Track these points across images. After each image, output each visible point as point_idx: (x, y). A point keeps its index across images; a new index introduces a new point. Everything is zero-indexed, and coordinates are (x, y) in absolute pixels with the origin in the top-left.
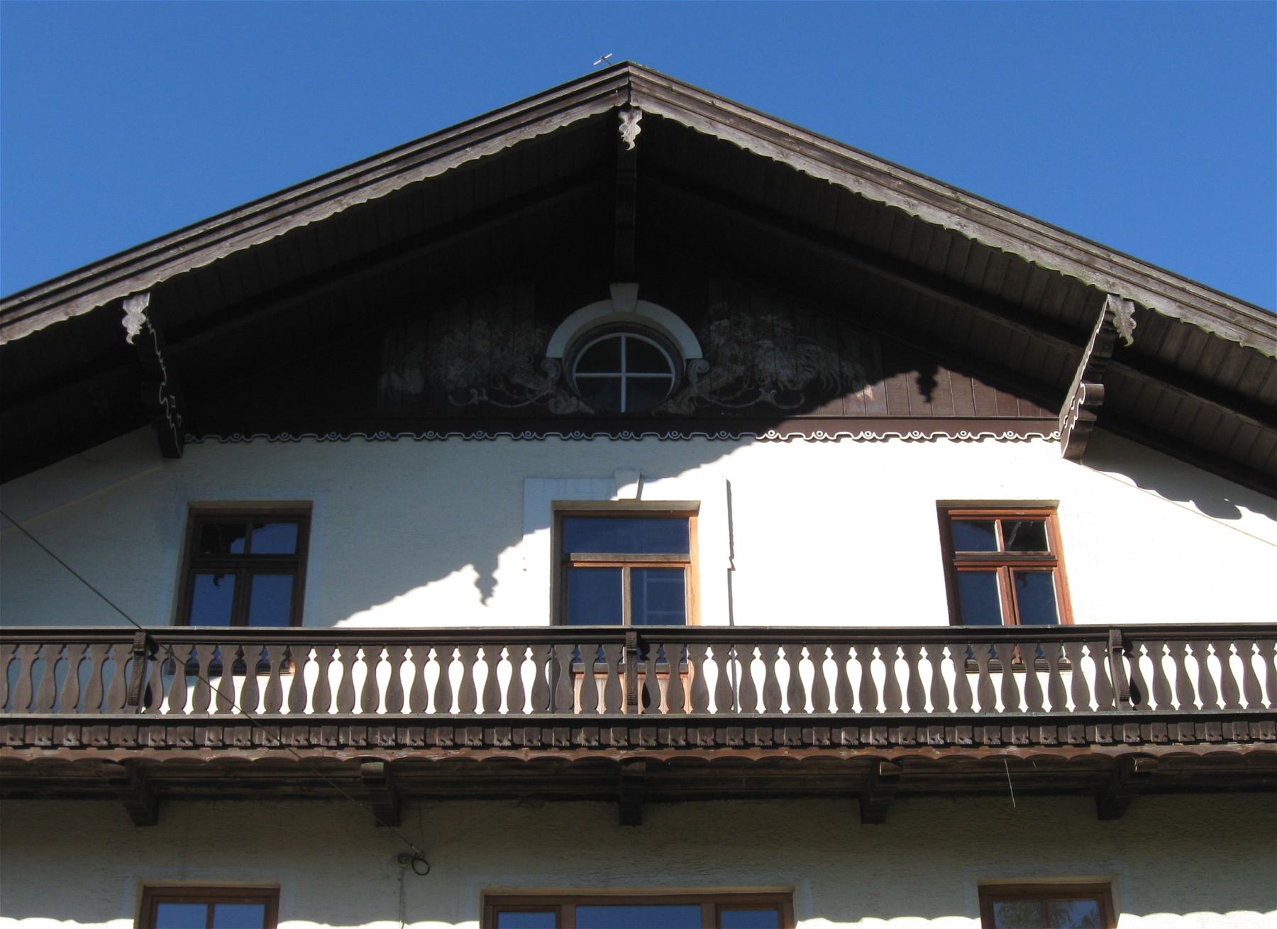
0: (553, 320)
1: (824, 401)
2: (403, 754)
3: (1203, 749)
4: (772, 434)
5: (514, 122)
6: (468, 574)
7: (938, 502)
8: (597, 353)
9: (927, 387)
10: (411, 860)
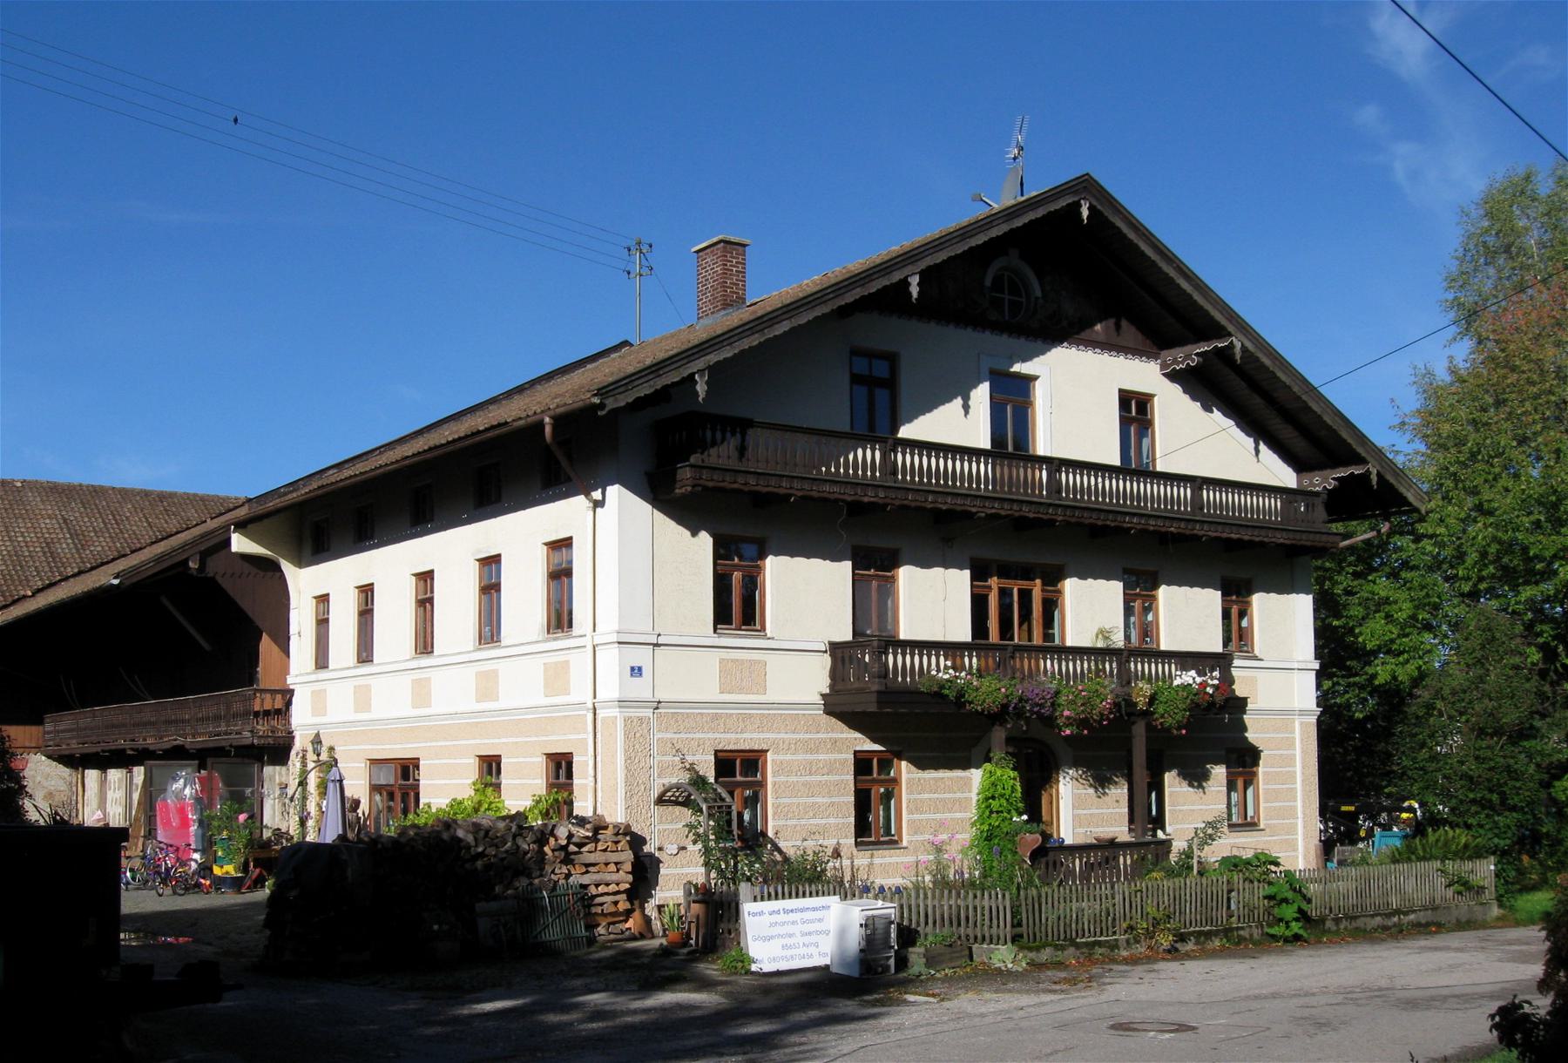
3: (1225, 535)
6: (959, 401)
7: (1121, 391)
8: (998, 284)
9: (1118, 327)
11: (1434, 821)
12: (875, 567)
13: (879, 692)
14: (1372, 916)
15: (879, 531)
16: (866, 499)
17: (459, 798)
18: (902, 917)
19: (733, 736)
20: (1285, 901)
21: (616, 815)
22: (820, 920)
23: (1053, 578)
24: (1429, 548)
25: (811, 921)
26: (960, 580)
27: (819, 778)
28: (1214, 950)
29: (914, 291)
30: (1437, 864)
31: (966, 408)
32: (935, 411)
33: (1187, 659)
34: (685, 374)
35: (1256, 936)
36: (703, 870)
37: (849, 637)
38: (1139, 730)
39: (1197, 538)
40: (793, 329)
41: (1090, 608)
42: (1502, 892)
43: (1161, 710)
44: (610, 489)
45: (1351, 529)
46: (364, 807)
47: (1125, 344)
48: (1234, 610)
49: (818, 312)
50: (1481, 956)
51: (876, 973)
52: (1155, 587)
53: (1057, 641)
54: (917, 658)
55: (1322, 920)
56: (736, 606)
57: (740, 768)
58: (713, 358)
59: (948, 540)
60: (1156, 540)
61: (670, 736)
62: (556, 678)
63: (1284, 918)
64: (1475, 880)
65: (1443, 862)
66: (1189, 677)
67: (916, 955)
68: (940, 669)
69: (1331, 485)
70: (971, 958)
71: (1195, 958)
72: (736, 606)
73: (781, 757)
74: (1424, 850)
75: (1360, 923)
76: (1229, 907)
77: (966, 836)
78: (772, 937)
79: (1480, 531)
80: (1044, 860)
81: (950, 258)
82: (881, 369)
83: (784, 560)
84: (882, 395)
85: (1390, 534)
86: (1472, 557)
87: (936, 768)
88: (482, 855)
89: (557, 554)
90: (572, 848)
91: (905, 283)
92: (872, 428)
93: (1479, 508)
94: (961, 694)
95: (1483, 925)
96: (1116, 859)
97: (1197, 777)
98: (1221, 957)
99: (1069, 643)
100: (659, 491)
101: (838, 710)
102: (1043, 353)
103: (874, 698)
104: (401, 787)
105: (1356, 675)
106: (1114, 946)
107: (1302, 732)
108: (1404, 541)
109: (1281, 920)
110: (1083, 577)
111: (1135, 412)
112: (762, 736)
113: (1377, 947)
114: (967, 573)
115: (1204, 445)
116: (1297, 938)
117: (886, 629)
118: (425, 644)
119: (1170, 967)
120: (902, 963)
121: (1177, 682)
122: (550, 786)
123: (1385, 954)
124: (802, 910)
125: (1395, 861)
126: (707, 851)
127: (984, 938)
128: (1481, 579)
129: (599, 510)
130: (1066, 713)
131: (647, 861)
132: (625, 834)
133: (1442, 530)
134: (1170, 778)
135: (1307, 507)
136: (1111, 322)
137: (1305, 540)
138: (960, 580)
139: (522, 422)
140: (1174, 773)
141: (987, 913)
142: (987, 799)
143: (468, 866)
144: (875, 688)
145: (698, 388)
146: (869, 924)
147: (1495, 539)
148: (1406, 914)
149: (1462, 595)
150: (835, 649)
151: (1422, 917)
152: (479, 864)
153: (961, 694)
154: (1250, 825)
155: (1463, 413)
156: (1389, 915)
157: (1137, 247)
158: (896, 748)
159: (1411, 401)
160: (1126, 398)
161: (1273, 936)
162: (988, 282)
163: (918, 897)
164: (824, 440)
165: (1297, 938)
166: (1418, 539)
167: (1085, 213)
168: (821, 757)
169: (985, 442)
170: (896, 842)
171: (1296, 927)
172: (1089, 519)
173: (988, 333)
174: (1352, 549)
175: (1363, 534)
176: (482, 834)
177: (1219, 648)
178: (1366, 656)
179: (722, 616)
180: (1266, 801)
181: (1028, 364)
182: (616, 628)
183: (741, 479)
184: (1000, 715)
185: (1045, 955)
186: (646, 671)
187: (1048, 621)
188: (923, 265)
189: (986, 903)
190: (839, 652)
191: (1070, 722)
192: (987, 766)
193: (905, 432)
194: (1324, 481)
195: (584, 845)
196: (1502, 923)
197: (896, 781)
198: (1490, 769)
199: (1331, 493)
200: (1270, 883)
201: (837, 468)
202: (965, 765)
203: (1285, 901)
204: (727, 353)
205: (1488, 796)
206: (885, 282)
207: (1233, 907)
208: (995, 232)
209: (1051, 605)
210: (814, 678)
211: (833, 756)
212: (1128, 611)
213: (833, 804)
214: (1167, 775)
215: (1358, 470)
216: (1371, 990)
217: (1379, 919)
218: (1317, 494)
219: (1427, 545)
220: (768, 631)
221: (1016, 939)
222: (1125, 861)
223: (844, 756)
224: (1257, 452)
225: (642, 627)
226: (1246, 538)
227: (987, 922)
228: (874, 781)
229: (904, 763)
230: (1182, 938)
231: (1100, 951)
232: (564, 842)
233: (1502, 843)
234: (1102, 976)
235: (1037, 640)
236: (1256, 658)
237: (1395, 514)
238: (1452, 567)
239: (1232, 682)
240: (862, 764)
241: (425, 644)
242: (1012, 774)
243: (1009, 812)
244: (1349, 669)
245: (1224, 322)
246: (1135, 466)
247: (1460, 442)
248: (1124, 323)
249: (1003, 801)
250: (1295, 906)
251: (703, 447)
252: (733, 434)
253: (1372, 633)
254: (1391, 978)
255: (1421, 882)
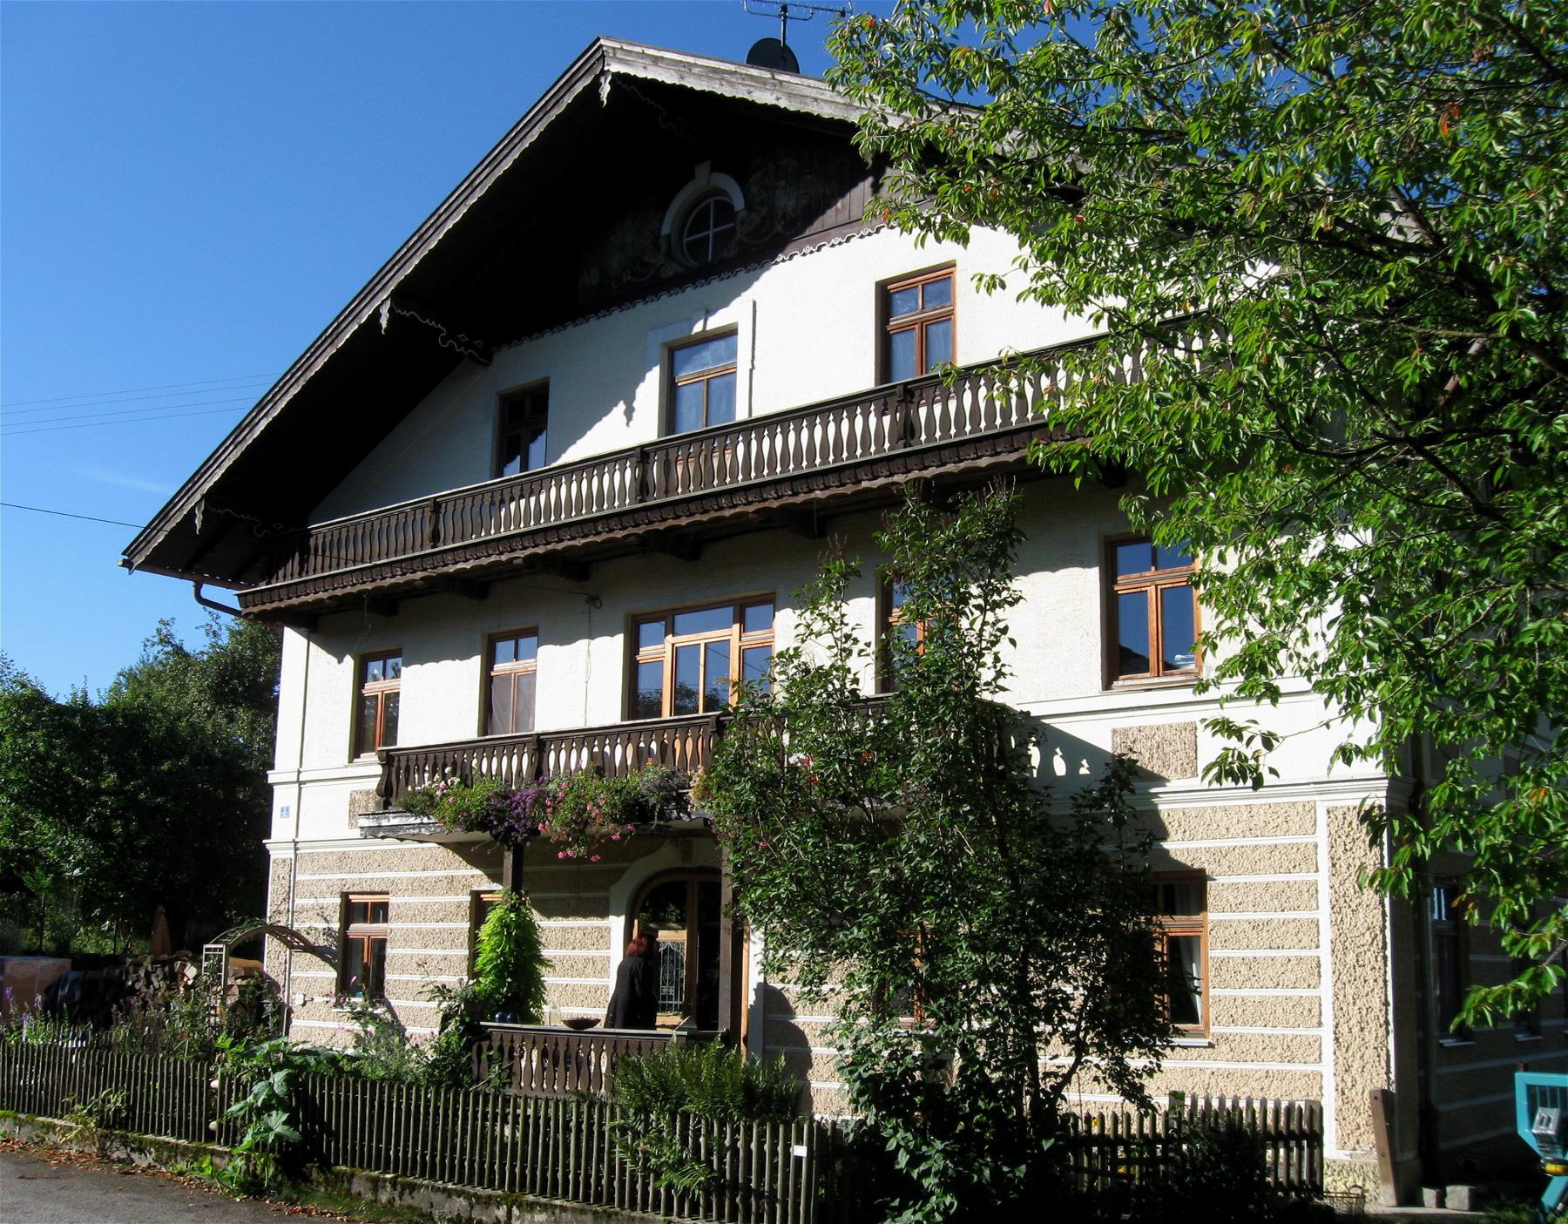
0: (664, 206)
1: (811, 223)
4: (780, 257)
5: (545, 110)
8: (696, 220)
10: (594, 600)
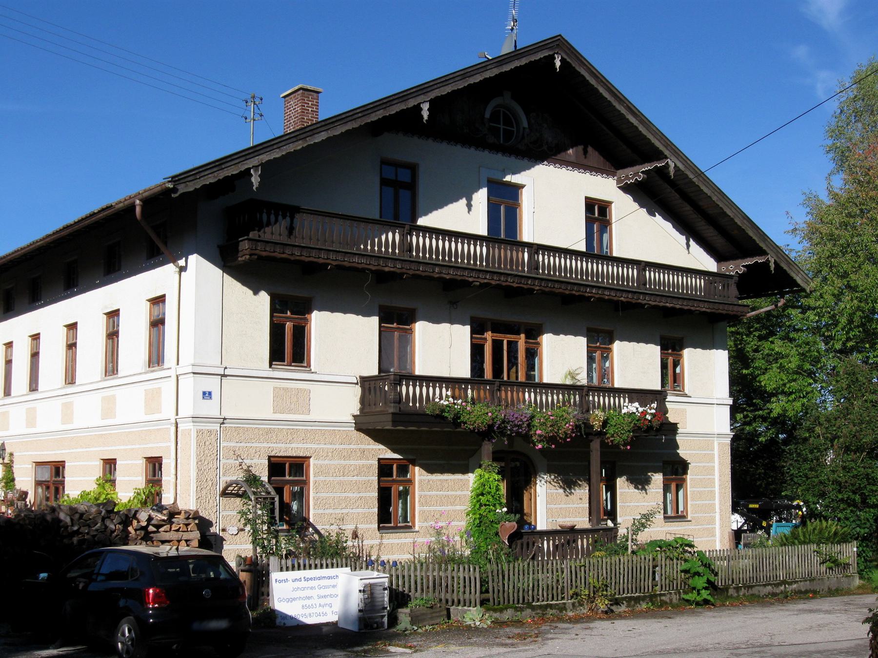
2: (486, 281)
3: (661, 304)
4: (545, 163)
6: (463, 201)
7: (587, 198)
8: (495, 116)
9: (585, 152)
11: (813, 514)
12: (396, 320)
13: (393, 414)
14: (765, 585)
15: (399, 295)
16: (387, 269)
17: (88, 490)
18: (391, 582)
19: (283, 445)
20: (698, 574)
21: (188, 503)
22: (334, 586)
23: (534, 333)
24: (812, 317)
25: (326, 587)
26: (461, 334)
27: (350, 478)
28: (641, 612)
29: (425, 114)
30: (814, 547)
31: (469, 206)
32: (446, 208)
33: (635, 394)
34: (243, 168)
35: (674, 601)
36: (251, 546)
37: (375, 372)
38: (595, 445)
39: (642, 306)
40: (329, 139)
41: (562, 356)
42: (862, 567)
43: (611, 431)
44: (190, 257)
45: (757, 305)
46: (31, 498)
47: (589, 164)
48: (670, 360)
49: (349, 126)
50: (843, 617)
51: (372, 628)
52: (611, 342)
53: (537, 381)
54: (424, 389)
55: (726, 589)
56: (288, 347)
57: (288, 470)
58: (265, 158)
59: (453, 303)
60: (611, 308)
61: (233, 444)
62: (152, 400)
63: (702, 587)
64: (842, 559)
65: (818, 545)
66: (634, 408)
67: (404, 615)
68: (443, 397)
69: (741, 271)
70: (449, 617)
71: (625, 618)
72: (288, 347)
73: (321, 462)
74: (804, 536)
75: (755, 591)
76: (654, 579)
77: (462, 524)
78: (294, 599)
79: (848, 303)
80: (519, 542)
81: (453, 91)
82: (404, 176)
83: (326, 314)
84: (405, 195)
85: (786, 307)
86: (843, 320)
87: (442, 472)
88: (77, 532)
89: (156, 308)
90: (151, 528)
91: (418, 108)
92: (396, 217)
93: (848, 286)
94: (457, 416)
95: (849, 593)
96: (575, 541)
97: (641, 482)
98: (645, 617)
99: (545, 381)
100: (227, 260)
101: (364, 428)
102: (529, 168)
103: (390, 418)
104: (55, 483)
105: (761, 409)
106: (563, 608)
107: (720, 451)
108: (794, 312)
109: (694, 588)
110: (556, 333)
111: (597, 213)
112: (305, 446)
113: (766, 610)
114: (468, 328)
115: (645, 237)
116: (706, 602)
117: (405, 368)
118: (70, 378)
119: (603, 626)
120: (393, 620)
121: (624, 411)
122: (148, 481)
123: (771, 615)
124: (320, 578)
125: (783, 544)
126: (255, 532)
127: (453, 601)
128: (848, 339)
129: (183, 273)
130: (539, 432)
131: (212, 539)
132: (194, 518)
133: (820, 303)
134: (621, 483)
135: (724, 286)
136: (580, 148)
137: (722, 309)
138: (461, 334)
139: (121, 205)
140: (624, 478)
141: (462, 582)
142: (478, 495)
143: (66, 541)
144: (391, 410)
145: (253, 179)
146: (369, 591)
147: (859, 308)
148: (790, 584)
149: (836, 351)
150: (365, 382)
151: (803, 586)
152: (75, 539)
153: (457, 416)
154: (679, 517)
155: (837, 220)
156: (777, 585)
157: (597, 90)
158: (411, 457)
159: (802, 217)
160: (590, 204)
161: (687, 601)
162: (487, 115)
163: (409, 570)
164: (355, 224)
165: (706, 602)
166: (805, 309)
167: (558, 64)
168: (352, 462)
169: (483, 231)
170: (410, 527)
171: (705, 594)
172: (558, 289)
173: (486, 152)
174: (758, 319)
175: (765, 306)
176: (77, 516)
177: (658, 387)
178: (767, 396)
179: (276, 355)
180: (693, 500)
181: (517, 176)
182: (192, 362)
183: (288, 251)
184: (488, 432)
185: (507, 615)
186: (216, 395)
187: (531, 367)
188: (433, 95)
189: (461, 575)
190: (367, 384)
191: (542, 439)
192: (478, 471)
193: (422, 221)
194: (736, 268)
195: (162, 526)
196: (862, 590)
197: (411, 482)
198: (853, 477)
199: (741, 276)
200: (686, 561)
201: (373, 245)
202: (465, 470)
203: (698, 574)
204: (276, 154)
205: (853, 497)
206: (403, 106)
207: (657, 578)
208: (488, 74)
209: (532, 354)
210: (347, 404)
211: (364, 462)
212: (590, 359)
213: (361, 498)
214: (618, 480)
215: (761, 260)
216: (754, 646)
217: (770, 587)
218: (731, 277)
219: (811, 315)
220: (312, 367)
221: (483, 602)
222: (582, 543)
223: (370, 462)
224: (688, 246)
225: (212, 362)
226: (678, 306)
227: (462, 590)
228: (394, 481)
229: (417, 468)
230: (617, 602)
231: (550, 612)
232: (144, 524)
233: (862, 531)
234: (548, 632)
235: (522, 378)
236: (686, 396)
237: (787, 293)
238: (828, 330)
239: (666, 412)
240: (384, 468)
241: (70, 378)
242: (496, 477)
243: (494, 505)
244: (754, 405)
245: (661, 148)
246: (595, 252)
247: (832, 238)
248: (590, 149)
249: (489, 497)
250: (705, 578)
251: (260, 226)
252: (284, 217)
253: (769, 381)
254: (772, 636)
255: (801, 561)
